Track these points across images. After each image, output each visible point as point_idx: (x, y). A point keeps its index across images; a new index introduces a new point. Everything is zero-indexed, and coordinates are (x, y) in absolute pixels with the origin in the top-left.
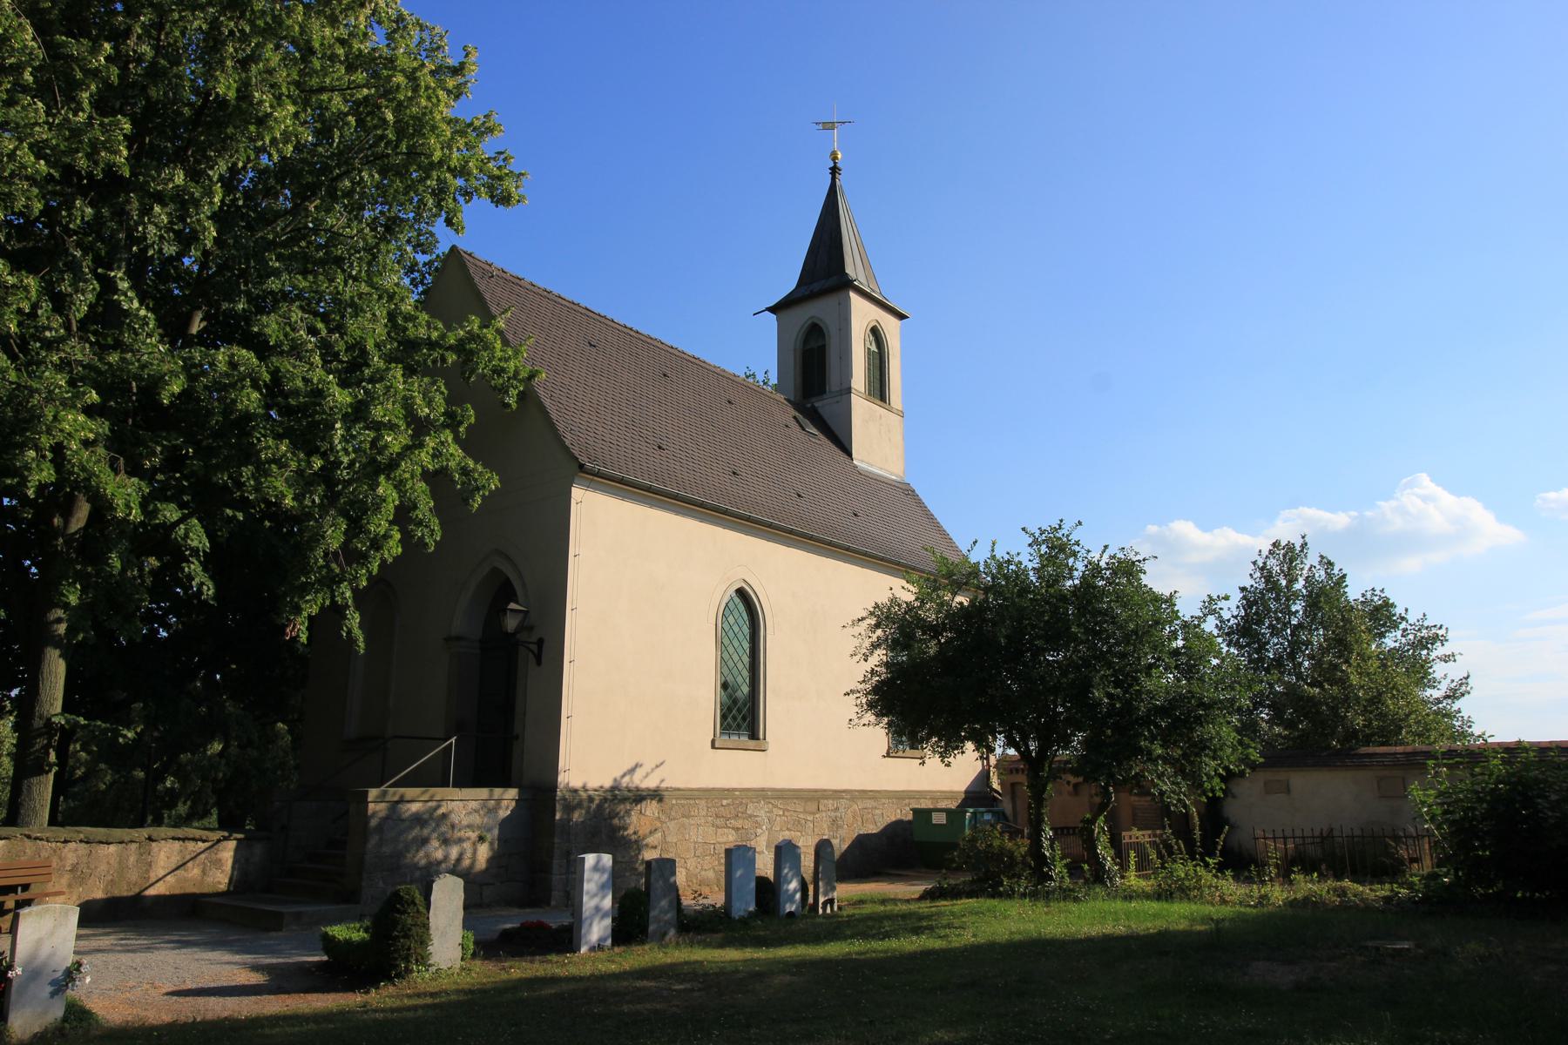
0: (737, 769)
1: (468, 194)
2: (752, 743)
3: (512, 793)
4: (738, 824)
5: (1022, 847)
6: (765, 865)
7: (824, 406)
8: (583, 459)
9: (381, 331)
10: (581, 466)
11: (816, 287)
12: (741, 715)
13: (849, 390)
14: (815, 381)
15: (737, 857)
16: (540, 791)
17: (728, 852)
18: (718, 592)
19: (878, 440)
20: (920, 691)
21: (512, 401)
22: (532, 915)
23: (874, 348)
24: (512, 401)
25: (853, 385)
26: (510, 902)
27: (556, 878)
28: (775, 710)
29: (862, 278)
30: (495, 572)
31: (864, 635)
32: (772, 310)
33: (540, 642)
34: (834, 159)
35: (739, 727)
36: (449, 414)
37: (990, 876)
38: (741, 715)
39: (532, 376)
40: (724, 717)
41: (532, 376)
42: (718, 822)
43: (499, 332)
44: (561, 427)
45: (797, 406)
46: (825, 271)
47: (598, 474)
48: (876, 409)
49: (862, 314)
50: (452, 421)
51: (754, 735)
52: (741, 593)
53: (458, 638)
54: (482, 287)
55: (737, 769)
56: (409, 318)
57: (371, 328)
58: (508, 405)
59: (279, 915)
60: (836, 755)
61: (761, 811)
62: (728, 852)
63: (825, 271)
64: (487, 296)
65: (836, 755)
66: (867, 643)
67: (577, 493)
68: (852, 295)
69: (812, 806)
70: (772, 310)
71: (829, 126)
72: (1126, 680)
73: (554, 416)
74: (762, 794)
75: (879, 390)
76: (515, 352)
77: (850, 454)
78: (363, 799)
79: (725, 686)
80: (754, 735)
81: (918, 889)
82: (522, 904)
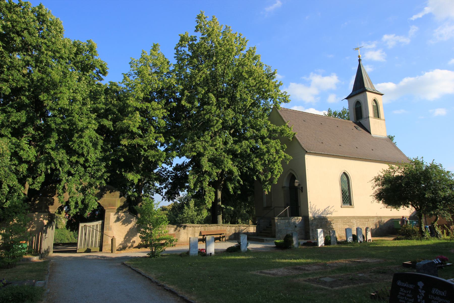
0: (347, 212)
1: (280, 103)
2: (350, 206)
3: (301, 218)
4: (349, 224)
5: (417, 229)
6: (355, 233)
7: (362, 121)
8: (307, 150)
9: (266, 131)
10: (307, 152)
11: (357, 92)
12: (347, 199)
13: (369, 117)
14: (358, 115)
15: (348, 231)
16: (306, 218)
17: (346, 229)
18: (339, 174)
19: (378, 128)
20: (392, 191)
21: (291, 139)
22: (309, 241)
23: (375, 104)
24: (291, 139)
25: (370, 115)
26: (302, 239)
27: (311, 234)
28: (355, 198)
29: (370, 87)
30: (291, 173)
31: (373, 183)
32: (346, 99)
33: (302, 188)
34: (359, 57)
35: (347, 203)
36: (282, 147)
37: (408, 235)
38: (347, 199)
39: (294, 134)
40: (343, 201)
41: (294, 134)
42: (345, 223)
43: (287, 126)
44: (301, 143)
45: (355, 123)
46: (360, 87)
47: (310, 153)
48: (377, 120)
49: (370, 97)
50: (282, 148)
51: (351, 205)
52: (344, 173)
53: (285, 187)
54: (281, 114)
55: (347, 212)
56: (270, 126)
57: (264, 132)
58: (290, 140)
59: (263, 240)
60: (368, 209)
61: (354, 221)
62: (346, 229)
63: (360, 87)
64: (282, 116)
65: (368, 209)
66: (374, 185)
67: (307, 157)
68: (367, 93)
69: (367, 220)
70: (346, 99)
71: (357, 49)
72: (435, 192)
73: (299, 141)
74: (354, 217)
75: (377, 115)
76: (291, 129)
77: (370, 133)
78: (274, 219)
79: (342, 191)
80: (351, 205)
81: (393, 238)
82: (305, 239)
